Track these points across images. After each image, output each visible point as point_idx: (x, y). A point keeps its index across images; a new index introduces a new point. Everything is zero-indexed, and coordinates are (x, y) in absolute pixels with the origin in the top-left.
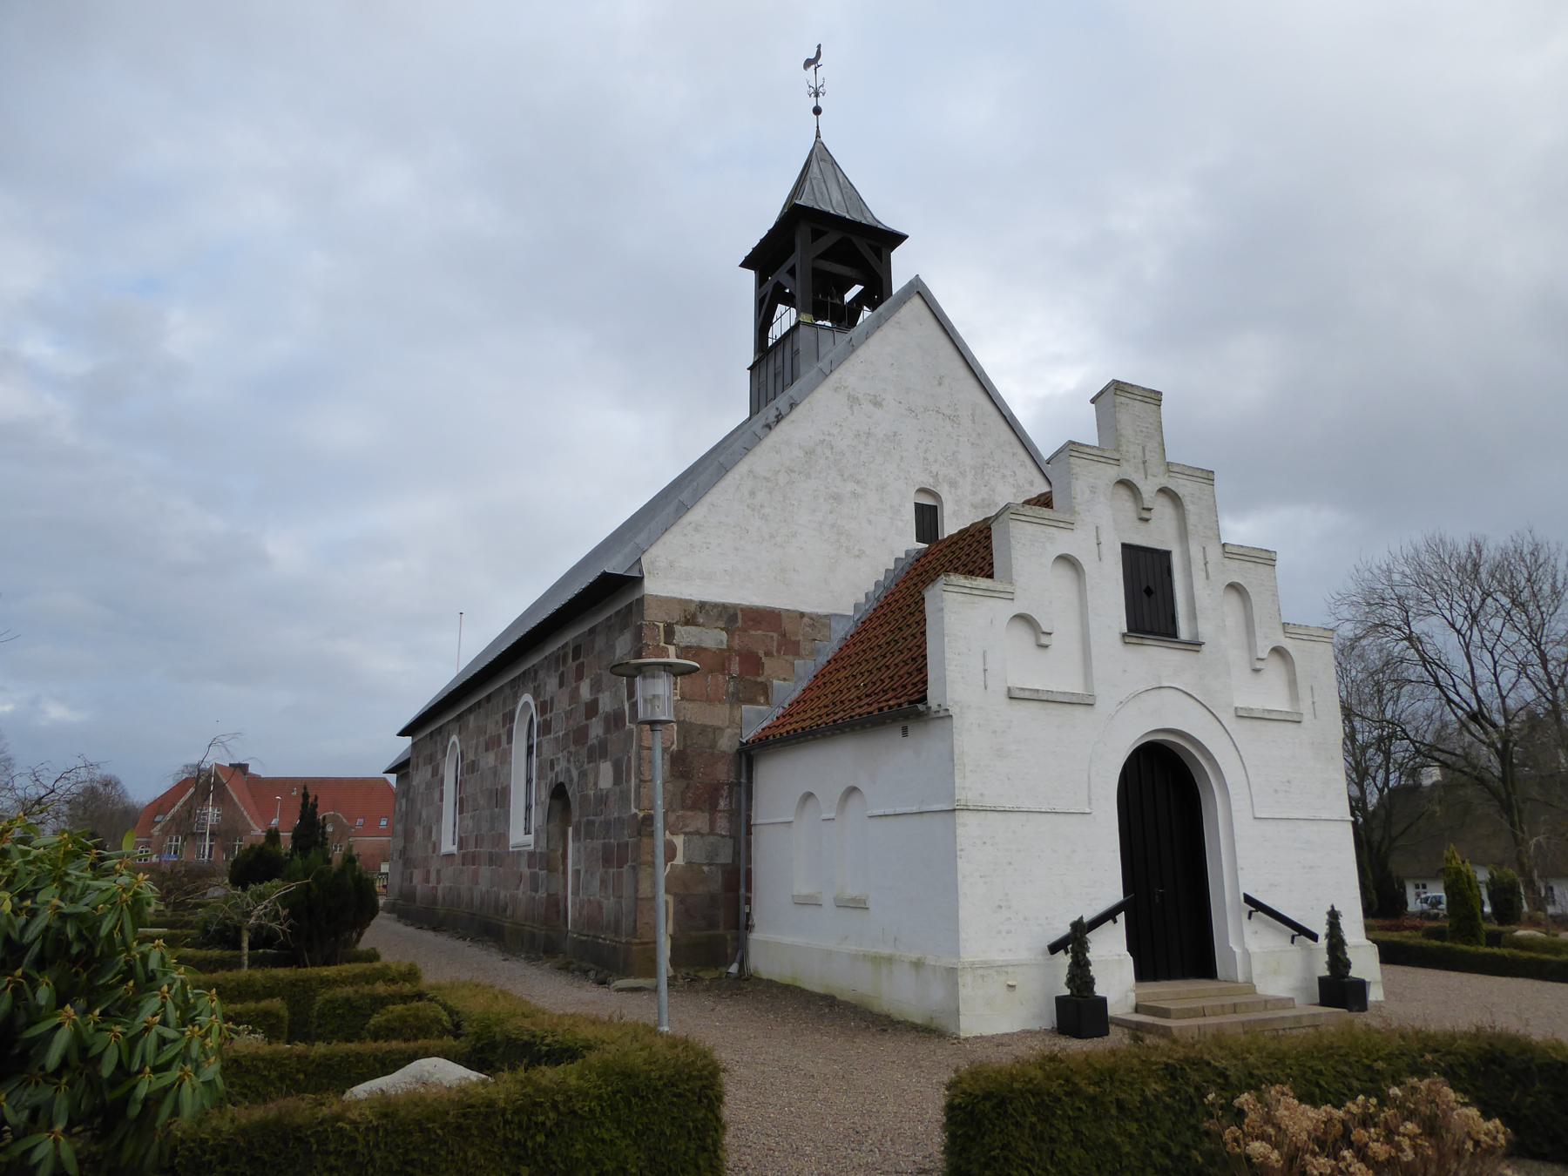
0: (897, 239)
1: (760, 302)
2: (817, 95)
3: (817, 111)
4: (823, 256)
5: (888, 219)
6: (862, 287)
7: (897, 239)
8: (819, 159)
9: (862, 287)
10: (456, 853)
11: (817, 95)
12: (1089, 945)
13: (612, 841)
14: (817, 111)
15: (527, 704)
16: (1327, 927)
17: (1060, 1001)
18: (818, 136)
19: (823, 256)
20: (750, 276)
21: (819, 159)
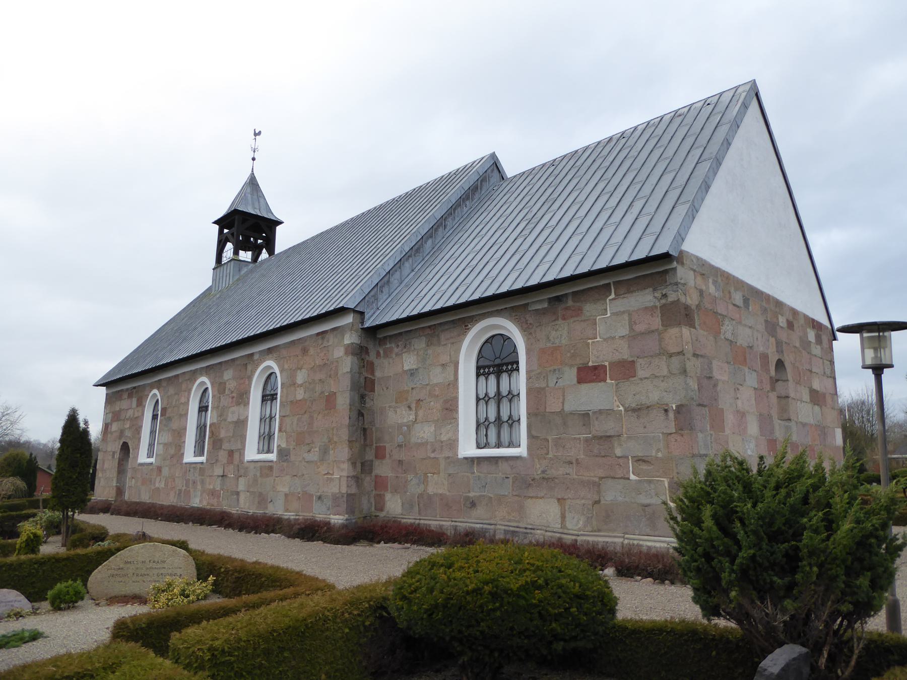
0: (279, 223)
1: (219, 242)
2: (254, 152)
3: (254, 159)
4: (247, 229)
5: (278, 214)
6: (264, 249)
7: (279, 223)
8: (252, 183)
9: (264, 249)
10: (205, 462)
11: (254, 152)
12: (23, 440)
13: (554, 625)
14: (254, 159)
15: (155, 395)
16: (67, 418)
17: (256, 533)
18: (252, 171)
19: (247, 229)
20: (217, 227)
21: (252, 183)
